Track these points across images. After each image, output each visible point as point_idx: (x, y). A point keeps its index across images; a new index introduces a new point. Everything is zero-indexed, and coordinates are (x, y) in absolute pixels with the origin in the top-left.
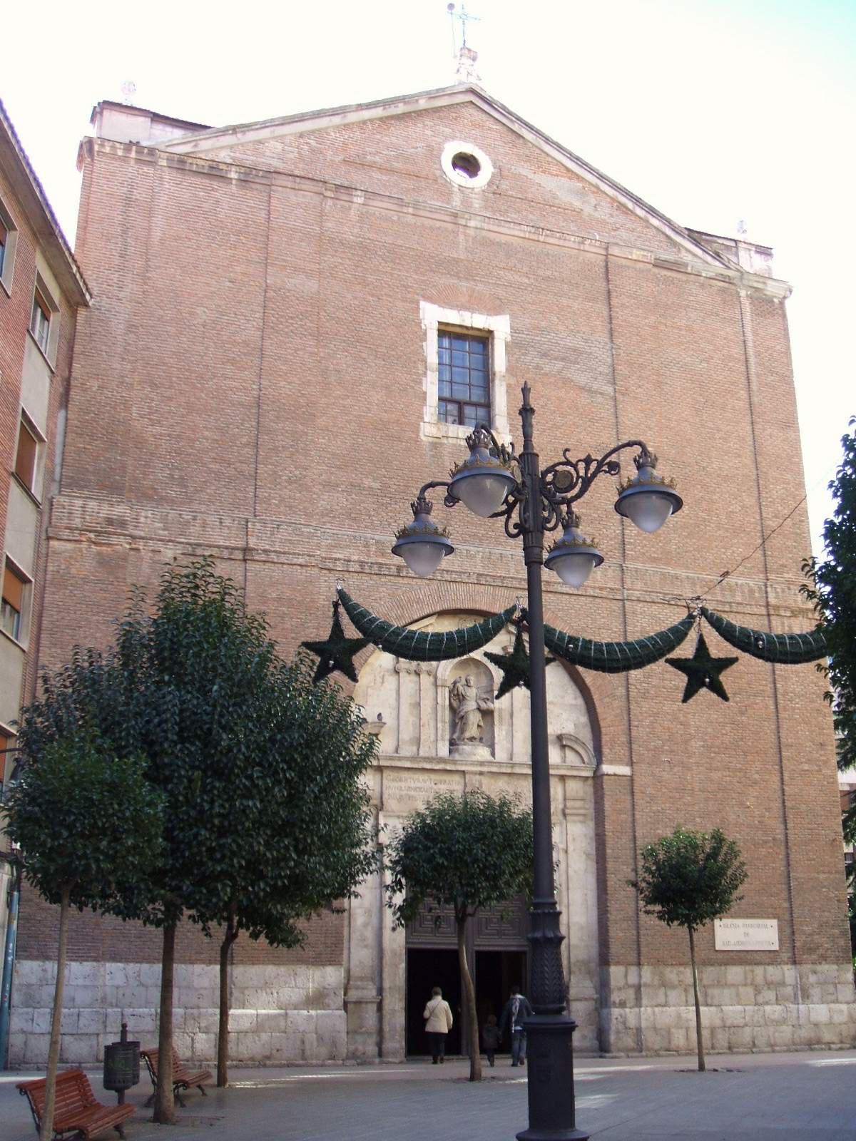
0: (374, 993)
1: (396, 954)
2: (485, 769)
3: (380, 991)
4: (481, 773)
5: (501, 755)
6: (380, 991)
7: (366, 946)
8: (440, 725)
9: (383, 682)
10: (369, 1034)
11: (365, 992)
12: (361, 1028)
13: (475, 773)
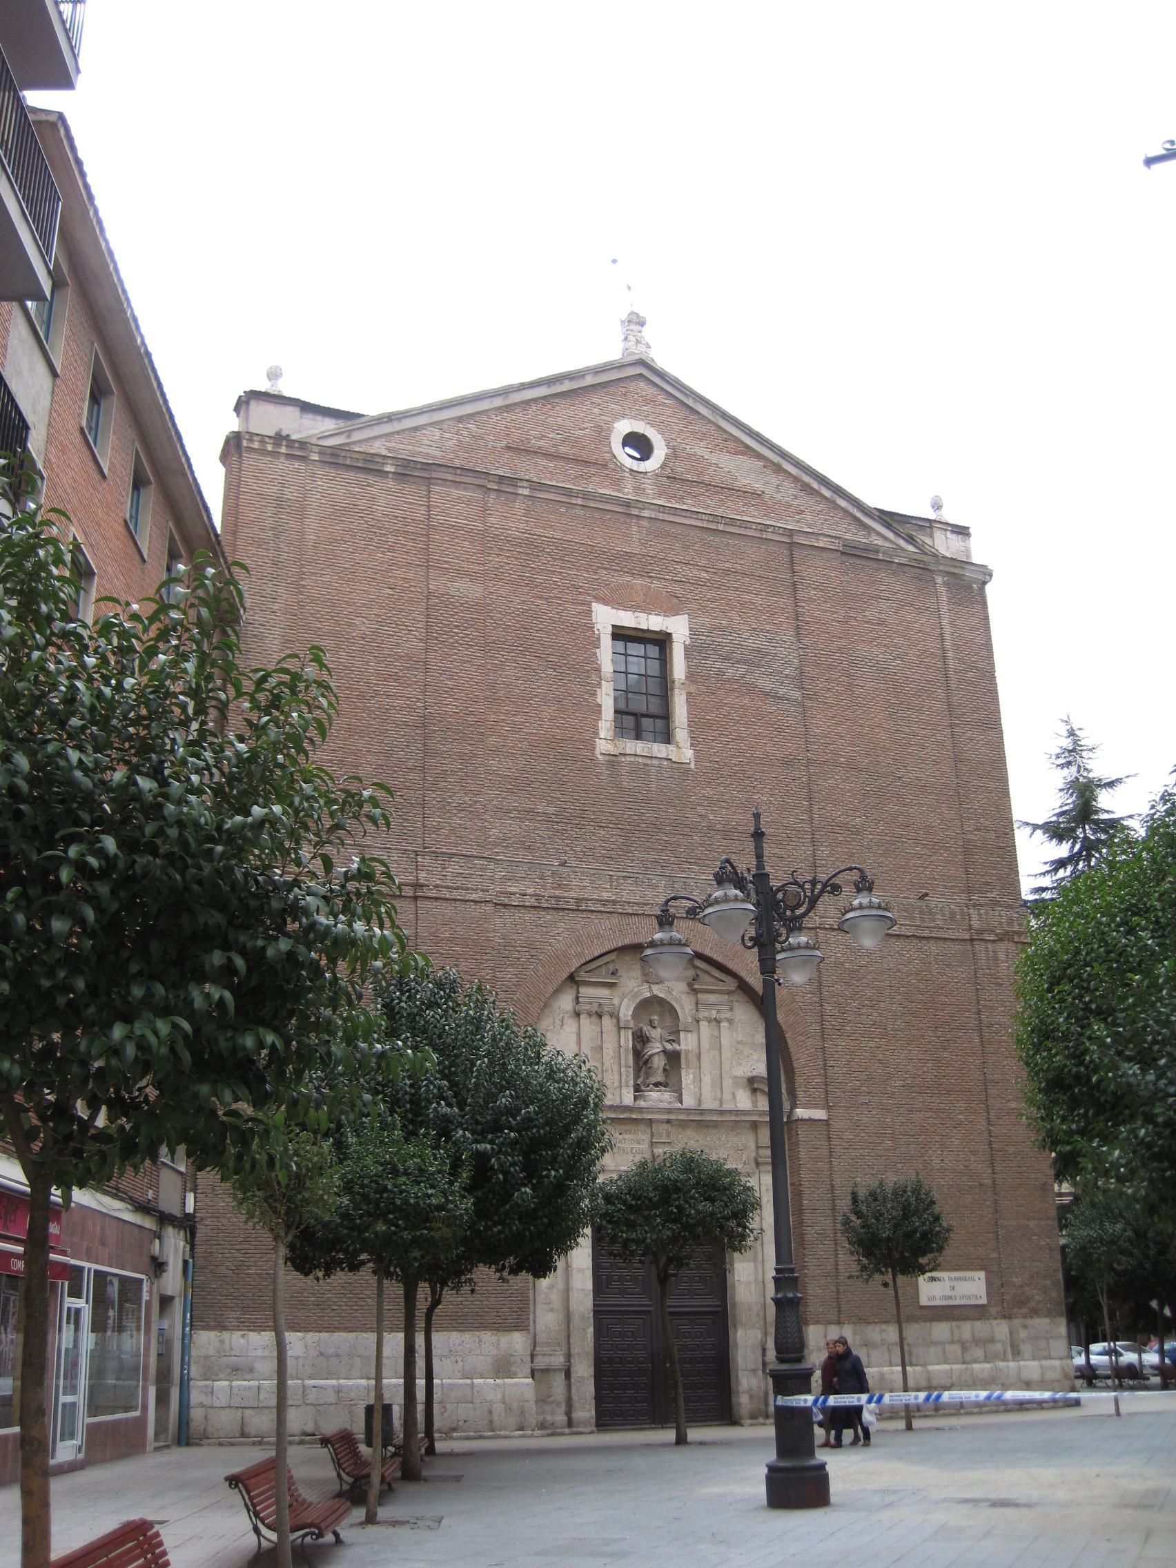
0: (562, 1359)
1: (583, 1317)
2: (672, 1117)
3: (568, 1356)
4: (668, 1121)
5: (689, 1101)
6: (568, 1356)
7: (552, 1310)
8: (623, 1070)
9: (562, 1025)
10: (558, 1404)
11: (552, 1359)
12: (549, 1397)
13: (661, 1122)
